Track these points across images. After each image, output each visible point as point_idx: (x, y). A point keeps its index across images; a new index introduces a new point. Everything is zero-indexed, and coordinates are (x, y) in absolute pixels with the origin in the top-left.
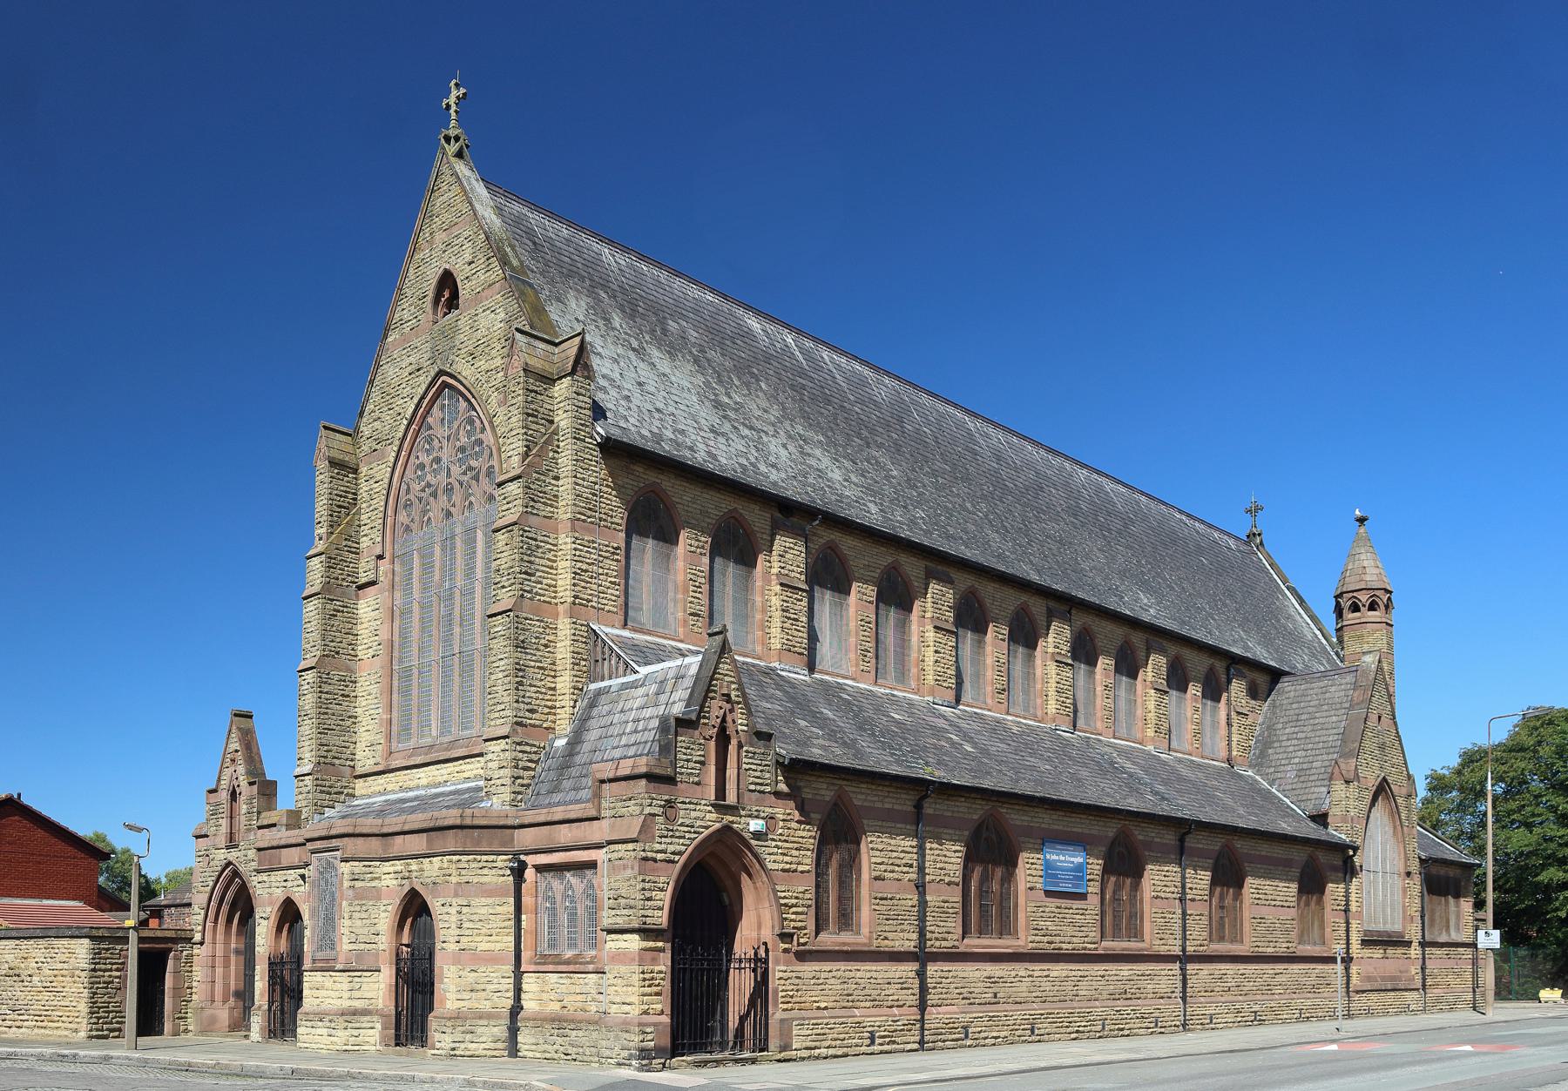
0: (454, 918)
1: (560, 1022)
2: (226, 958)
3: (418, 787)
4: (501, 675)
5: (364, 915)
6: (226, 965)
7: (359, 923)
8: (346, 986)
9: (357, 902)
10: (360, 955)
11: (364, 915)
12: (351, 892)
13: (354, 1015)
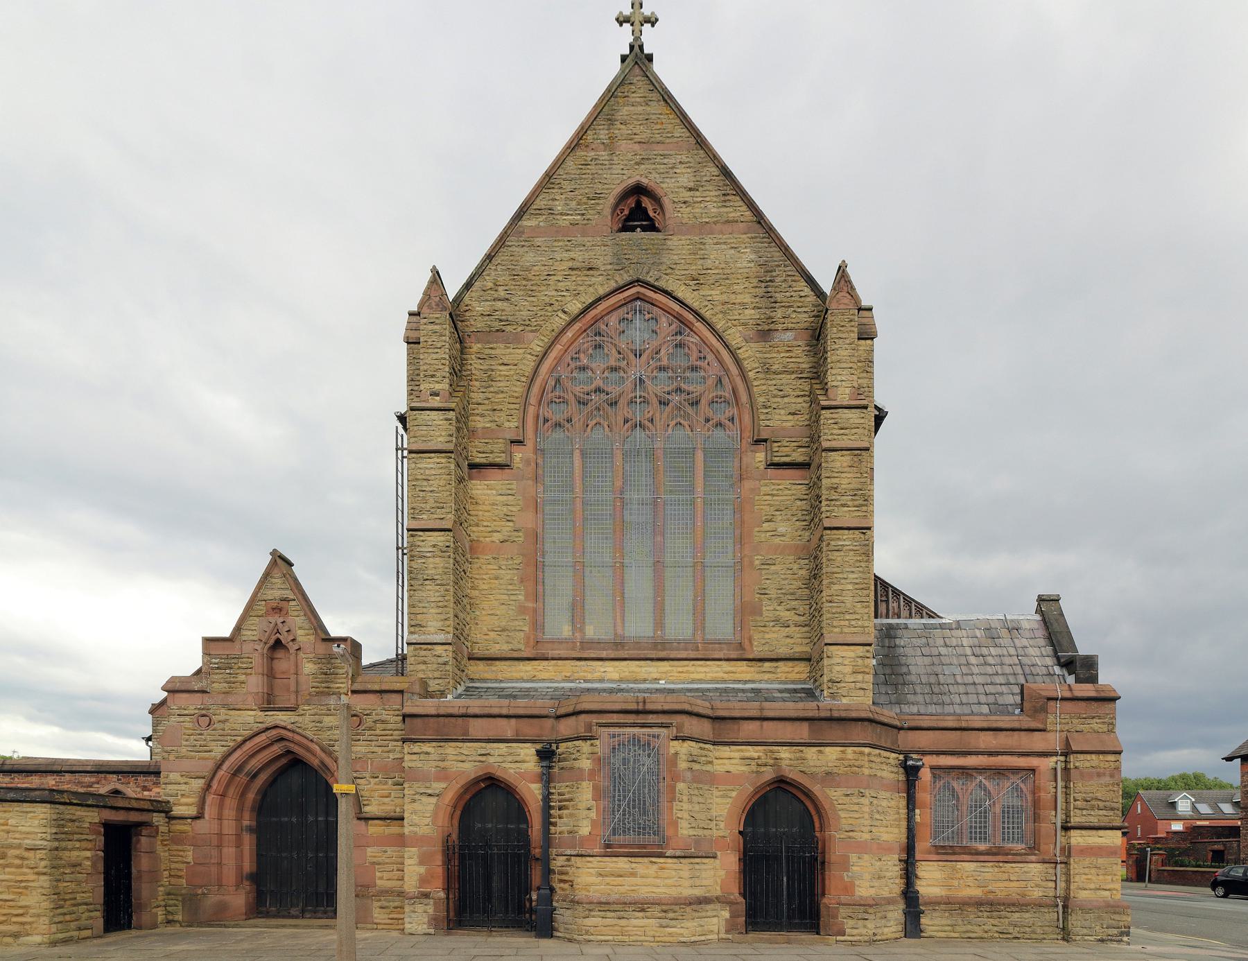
0: (866, 809)
1: (956, 906)
2: (238, 836)
3: (645, 681)
4: (850, 587)
5: (701, 800)
6: (239, 845)
7: (697, 807)
8: (686, 874)
9: (695, 785)
10: (698, 841)
11: (701, 800)
12: (689, 774)
13: (700, 903)
